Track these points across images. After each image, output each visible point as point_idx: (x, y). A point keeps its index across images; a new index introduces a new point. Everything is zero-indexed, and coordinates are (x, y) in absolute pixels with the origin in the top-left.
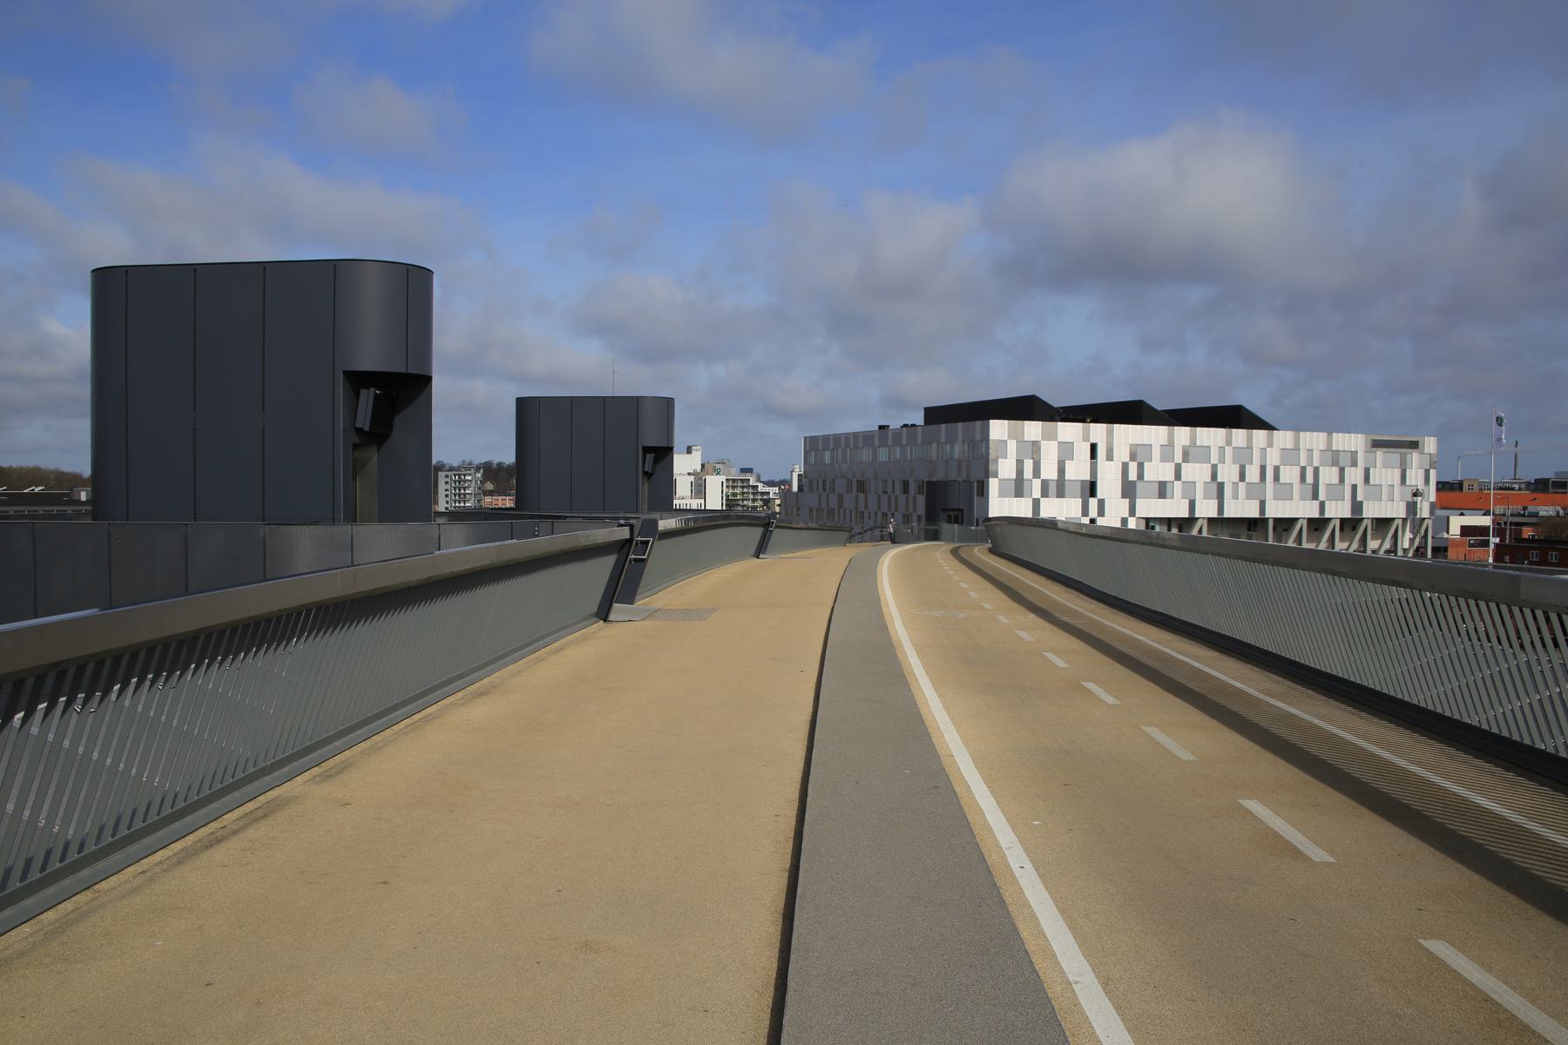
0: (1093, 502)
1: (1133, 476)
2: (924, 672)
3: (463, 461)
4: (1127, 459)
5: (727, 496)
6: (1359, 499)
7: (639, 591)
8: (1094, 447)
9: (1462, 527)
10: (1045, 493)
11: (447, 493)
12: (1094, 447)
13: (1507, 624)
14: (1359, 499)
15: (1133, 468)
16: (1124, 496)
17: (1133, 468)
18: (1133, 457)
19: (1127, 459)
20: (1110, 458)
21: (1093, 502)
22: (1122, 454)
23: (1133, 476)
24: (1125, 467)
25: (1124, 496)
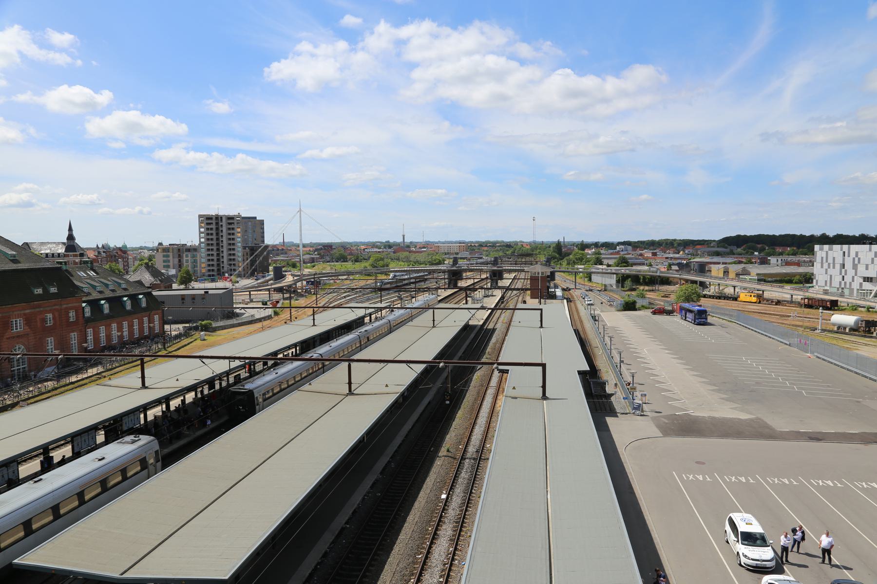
0: (843, 270)
1: (856, 262)
2: (633, 485)
3: (160, 244)
4: (854, 257)
5: (430, 265)
6: (856, 263)
7: (127, 472)
8: (844, 252)
9: (263, 220)
10: (829, 267)
11: (753, 296)
12: (844, 252)
13: (498, 317)
14: (856, 263)
15: (856, 259)
16: (853, 269)
17: (856, 259)
18: (857, 255)
19: (854, 257)
20: (849, 256)
21: (843, 270)
22: (853, 255)
23: (856, 262)
24: (854, 259)
25: (853, 269)
